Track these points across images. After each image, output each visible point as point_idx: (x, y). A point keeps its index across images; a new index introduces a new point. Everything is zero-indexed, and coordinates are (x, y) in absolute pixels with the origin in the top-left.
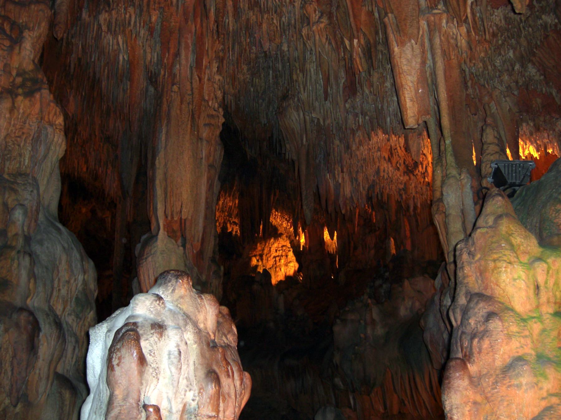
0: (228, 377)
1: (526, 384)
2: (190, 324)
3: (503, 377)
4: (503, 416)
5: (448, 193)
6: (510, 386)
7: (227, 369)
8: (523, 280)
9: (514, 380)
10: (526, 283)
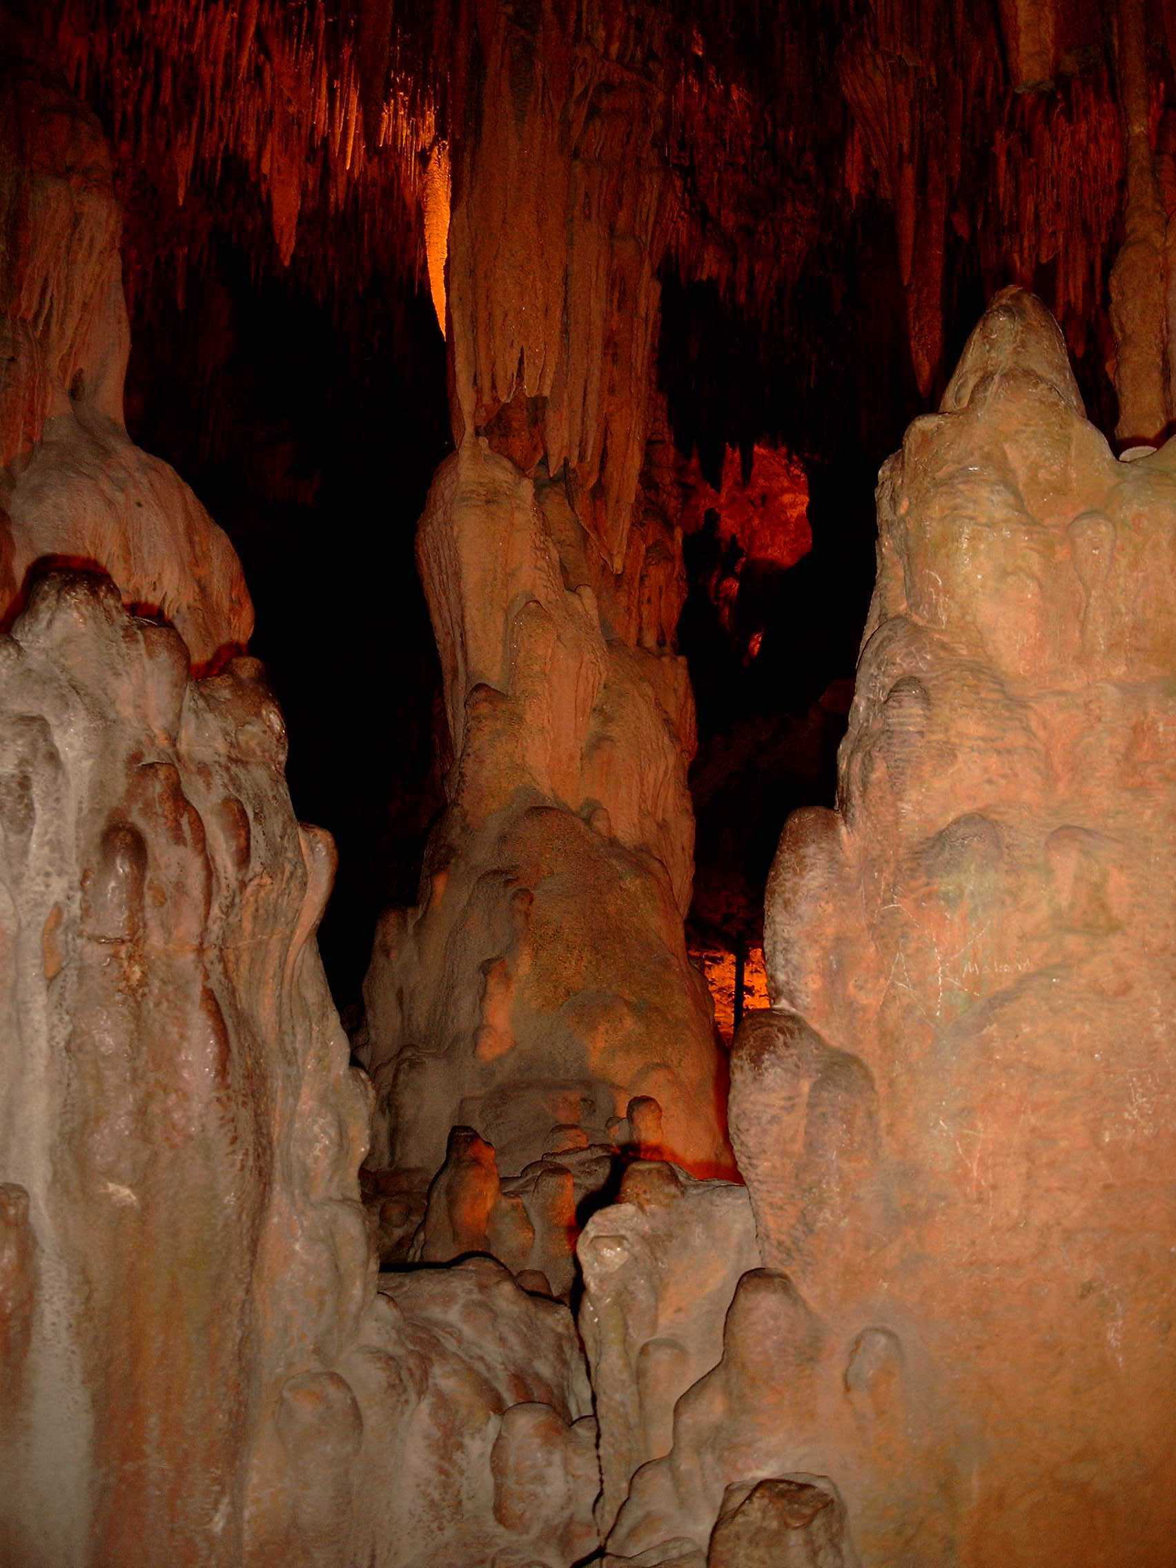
0: (177, 843)
1: (972, 893)
2: (80, 706)
3: (912, 870)
4: (903, 981)
5: (1123, 294)
6: (929, 896)
7: (177, 821)
8: (1033, 576)
9: (939, 879)
10: (1041, 586)
